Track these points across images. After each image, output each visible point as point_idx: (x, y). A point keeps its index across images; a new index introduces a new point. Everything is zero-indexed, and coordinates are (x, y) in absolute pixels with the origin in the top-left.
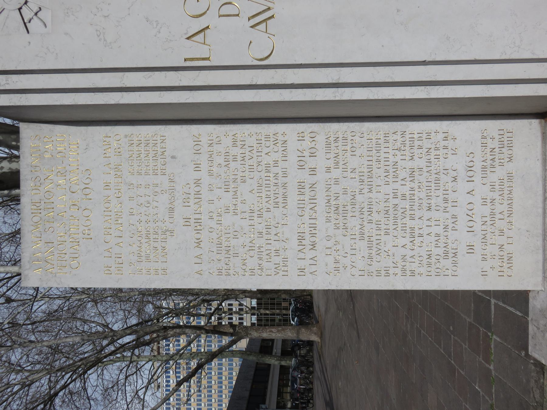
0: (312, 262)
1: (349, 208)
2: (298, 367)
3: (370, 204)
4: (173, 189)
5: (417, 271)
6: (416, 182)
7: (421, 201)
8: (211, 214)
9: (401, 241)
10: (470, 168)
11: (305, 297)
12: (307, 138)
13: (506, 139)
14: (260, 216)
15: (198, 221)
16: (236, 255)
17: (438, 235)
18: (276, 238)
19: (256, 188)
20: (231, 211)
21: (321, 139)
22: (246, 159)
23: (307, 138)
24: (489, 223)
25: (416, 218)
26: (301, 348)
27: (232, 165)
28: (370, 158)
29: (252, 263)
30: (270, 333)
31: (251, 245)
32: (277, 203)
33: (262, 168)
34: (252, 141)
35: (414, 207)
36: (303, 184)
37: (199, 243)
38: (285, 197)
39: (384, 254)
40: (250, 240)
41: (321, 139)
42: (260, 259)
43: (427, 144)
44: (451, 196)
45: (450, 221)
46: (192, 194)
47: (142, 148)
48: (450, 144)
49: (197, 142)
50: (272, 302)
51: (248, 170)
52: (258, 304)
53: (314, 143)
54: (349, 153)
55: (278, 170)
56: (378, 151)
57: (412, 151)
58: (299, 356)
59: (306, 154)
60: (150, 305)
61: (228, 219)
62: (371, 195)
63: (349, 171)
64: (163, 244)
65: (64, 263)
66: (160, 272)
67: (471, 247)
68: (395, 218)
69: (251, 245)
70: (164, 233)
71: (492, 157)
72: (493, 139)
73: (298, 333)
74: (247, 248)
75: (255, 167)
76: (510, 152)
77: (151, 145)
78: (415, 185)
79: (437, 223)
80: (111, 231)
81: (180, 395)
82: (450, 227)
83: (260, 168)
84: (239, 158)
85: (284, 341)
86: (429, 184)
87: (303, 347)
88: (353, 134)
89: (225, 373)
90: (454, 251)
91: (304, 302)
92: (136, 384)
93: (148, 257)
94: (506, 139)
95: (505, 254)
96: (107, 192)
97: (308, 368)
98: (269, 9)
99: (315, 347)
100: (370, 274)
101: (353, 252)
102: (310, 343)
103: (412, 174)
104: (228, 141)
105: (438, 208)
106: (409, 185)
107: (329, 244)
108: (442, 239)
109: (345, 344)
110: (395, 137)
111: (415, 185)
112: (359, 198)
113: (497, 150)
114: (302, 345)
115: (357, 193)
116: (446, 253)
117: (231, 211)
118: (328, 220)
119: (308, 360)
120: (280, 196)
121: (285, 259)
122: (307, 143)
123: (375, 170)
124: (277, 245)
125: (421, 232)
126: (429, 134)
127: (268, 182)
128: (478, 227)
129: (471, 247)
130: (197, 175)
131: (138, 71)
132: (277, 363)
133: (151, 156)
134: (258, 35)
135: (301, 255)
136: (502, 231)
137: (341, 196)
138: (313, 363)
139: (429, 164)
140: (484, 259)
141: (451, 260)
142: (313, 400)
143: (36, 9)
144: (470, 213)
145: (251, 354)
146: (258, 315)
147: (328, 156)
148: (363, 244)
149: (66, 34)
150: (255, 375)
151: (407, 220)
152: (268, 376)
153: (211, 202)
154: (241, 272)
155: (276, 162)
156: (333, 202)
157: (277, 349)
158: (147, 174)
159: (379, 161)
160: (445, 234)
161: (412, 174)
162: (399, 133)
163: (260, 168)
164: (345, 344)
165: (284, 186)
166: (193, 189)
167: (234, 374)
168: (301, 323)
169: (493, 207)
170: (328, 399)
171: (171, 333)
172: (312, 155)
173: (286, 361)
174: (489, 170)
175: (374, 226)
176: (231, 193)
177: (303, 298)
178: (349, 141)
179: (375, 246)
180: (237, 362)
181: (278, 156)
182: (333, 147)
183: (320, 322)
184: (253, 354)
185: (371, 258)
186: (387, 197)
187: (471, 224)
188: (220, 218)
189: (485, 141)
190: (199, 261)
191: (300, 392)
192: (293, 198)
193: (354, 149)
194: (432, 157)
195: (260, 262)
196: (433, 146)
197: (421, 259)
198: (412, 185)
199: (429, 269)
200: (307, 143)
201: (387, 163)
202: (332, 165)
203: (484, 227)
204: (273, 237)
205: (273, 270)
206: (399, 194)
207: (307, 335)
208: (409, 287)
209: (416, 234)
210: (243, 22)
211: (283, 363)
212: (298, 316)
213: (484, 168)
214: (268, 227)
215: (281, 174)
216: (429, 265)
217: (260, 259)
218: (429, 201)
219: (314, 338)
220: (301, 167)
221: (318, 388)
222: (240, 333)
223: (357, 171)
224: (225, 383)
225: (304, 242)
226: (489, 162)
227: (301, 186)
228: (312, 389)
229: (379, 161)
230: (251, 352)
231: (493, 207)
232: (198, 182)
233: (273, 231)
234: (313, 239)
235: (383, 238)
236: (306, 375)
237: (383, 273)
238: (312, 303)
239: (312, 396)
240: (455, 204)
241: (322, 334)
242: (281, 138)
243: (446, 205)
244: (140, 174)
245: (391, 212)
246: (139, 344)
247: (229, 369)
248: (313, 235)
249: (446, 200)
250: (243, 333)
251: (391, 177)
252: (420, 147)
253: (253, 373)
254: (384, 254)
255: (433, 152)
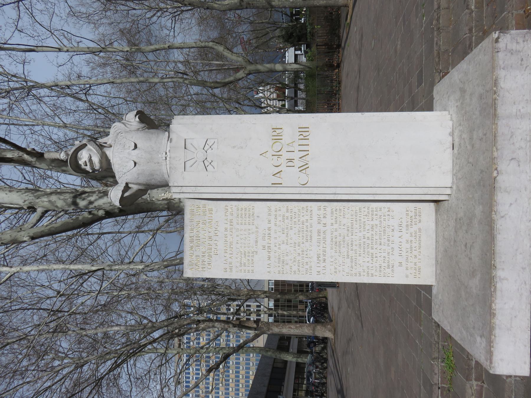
0: (324, 268)
1: (342, 243)
2: (313, 363)
3: (352, 241)
4: (257, 232)
5: (374, 274)
6: (374, 231)
7: (376, 240)
8: (275, 244)
9: (366, 260)
10: (400, 225)
11: (321, 299)
12: (322, 209)
13: (418, 212)
14: (299, 246)
15: (269, 247)
16: (287, 264)
17: (384, 257)
18: (307, 256)
19: (297, 232)
20: (285, 243)
21: (329, 210)
22: (293, 218)
23: (322, 209)
24: (409, 252)
25: (374, 249)
26: (316, 345)
27: (286, 221)
28: (352, 219)
29: (295, 268)
30: (289, 329)
31: (294, 259)
32: (307, 240)
33: (300, 223)
34: (296, 210)
35: (373, 243)
36: (320, 231)
37: (269, 258)
38: (311, 237)
39: (358, 266)
40: (294, 257)
41: (329, 210)
42: (299, 266)
43: (379, 213)
44: (391, 239)
45: (390, 251)
46: (267, 234)
47: (243, 212)
48: (391, 213)
49: (270, 210)
50: (289, 304)
51: (293, 223)
52: (275, 306)
53: (325, 211)
54: (342, 217)
55: (308, 224)
56: (356, 216)
57: (372, 216)
58: (315, 352)
59: (322, 216)
60: (177, 303)
61: (283, 247)
62: (352, 237)
63: (342, 225)
64: (252, 258)
65: (204, 266)
66: (250, 271)
67: (400, 263)
68: (364, 248)
69: (294, 259)
70: (253, 253)
71: (411, 220)
72: (411, 211)
73: (314, 330)
74: (292, 261)
75: (297, 222)
76: (420, 218)
77: (247, 210)
78: (374, 233)
79: (384, 251)
80: (227, 251)
81: (198, 391)
82: (391, 253)
83: (299, 223)
84: (289, 218)
85: (300, 338)
86: (381, 232)
87: (318, 344)
88: (344, 208)
89: (242, 372)
90: (392, 265)
91: (321, 303)
92: (165, 373)
93: (245, 264)
94: (418, 212)
95: (417, 267)
96: (226, 233)
97: (323, 363)
98: (307, 164)
99: (329, 344)
100: (351, 275)
101: (344, 264)
102: (325, 340)
103: (372, 228)
104: (284, 210)
105: (385, 244)
106: (371, 232)
107: (332, 260)
108: (387, 259)
109: (352, 335)
110: (364, 209)
111: (374, 233)
112: (346, 238)
113: (413, 217)
114: (318, 342)
115: (346, 236)
116: (389, 266)
117: (285, 243)
118: (332, 249)
119: (322, 356)
120: (309, 236)
121: (311, 267)
122: (322, 212)
123: (354, 225)
124: (306, 260)
125: (376, 255)
126: (381, 209)
127: (303, 230)
128: (404, 254)
129: (400, 263)
130: (269, 225)
131: (328, 283)
132: (294, 360)
133: (247, 215)
134: (302, 175)
135: (319, 265)
136: (416, 256)
137: (338, 237)
138: (327, 360)
139: (380, 223)
140: (407, 269)
141: (391, 269)
142: (326, 393)
143: (210, 161)
144: (400, 247)
145: (270, 351)
146: (275, 316)
147: (332, 218)
148: (349, 260)
149: (223, 172)
150: (272, 372)
151: (370, 249)
152: (285, 374)
153: (276, 238)
154: (289, 272)
155: (307, 220)
156: (334, 240)
157: (294, 345)
158: (245, 224)
159: (356, 221)
160: (388, 256)
161: (372, 228)
162: (366, 208)
163: (299, 223)
164: (353, 335)
165: (311, 231)
166: (267, 232)
167: (251, 373)
168: (316, 321)
169: (411, 244)
170: (339, 387)
171: (202, 326)
172: (324, 217)
173: (302, 358)
174: (410, 226)
175: (354, 252)
176: (285, 234)
177: (318, 299)
178: (342, 211)
179: (354, 261)
180: (254, 359)
181: (308, 217)
182: (334, 214)
183: (333, 321)
184: (271, 350)
185: (352, 267)
186: (360, 238)
187: (401, 252)
188: (280, 246)
189: (407, 212)
190: (269, 266)
191: (314, 385)
192: (315, 237)
193: (344, 215)
194: (382, 220)
195: (299, 268)
196: (383, 215)
197: (376, 268)
198: (372, 233)
199: (380, 273)
200: (322, 212)
201: (360, 222)
202: (334, 223)
203: (407, 254)
204: (305, 256)
205: (305, 271)
206: (366, 237)
207: (323, 332)
208: (370, 281)
209: (374, 256)
210: (296, 169)
211: (300, 360)
212: (314, 316)
213: (407, 225)
214: (303, 251)
215: (309, 226)
216: (380, 271)
217: (299, 266)
218: (380, 241)
219: (329, 335)
220: (319, 223)
221: (331, 382)
222: (263, 328)
223: (346, 225)
224: (242, 381)
225: (320, 259)
226: (409, 223)
227: (319, 232)
228: (326, 383)
229: (356, 221)
230: (270, 349)
231: (411, 244)
232: (269, 229)
233: (305, 253)
234: (324, 257)
235: (358, 258)
236: (321, 371)
237: (358, 275)
238: (327, 305)
239: (326, 389)
240: (393, 242)
241: (335, 330)
242: (309, 209)
243: (389, 243)
244: (242, 224)
245: (362, 245)
246: (169, 336)
247: (247, 368)
248: (324, 255)
249: (389, 240)
250: (265, 328)
251: (362, 228)
252: (376, 215)
253: (270, 370)
254: (358, 266)
255: (383, 217)
